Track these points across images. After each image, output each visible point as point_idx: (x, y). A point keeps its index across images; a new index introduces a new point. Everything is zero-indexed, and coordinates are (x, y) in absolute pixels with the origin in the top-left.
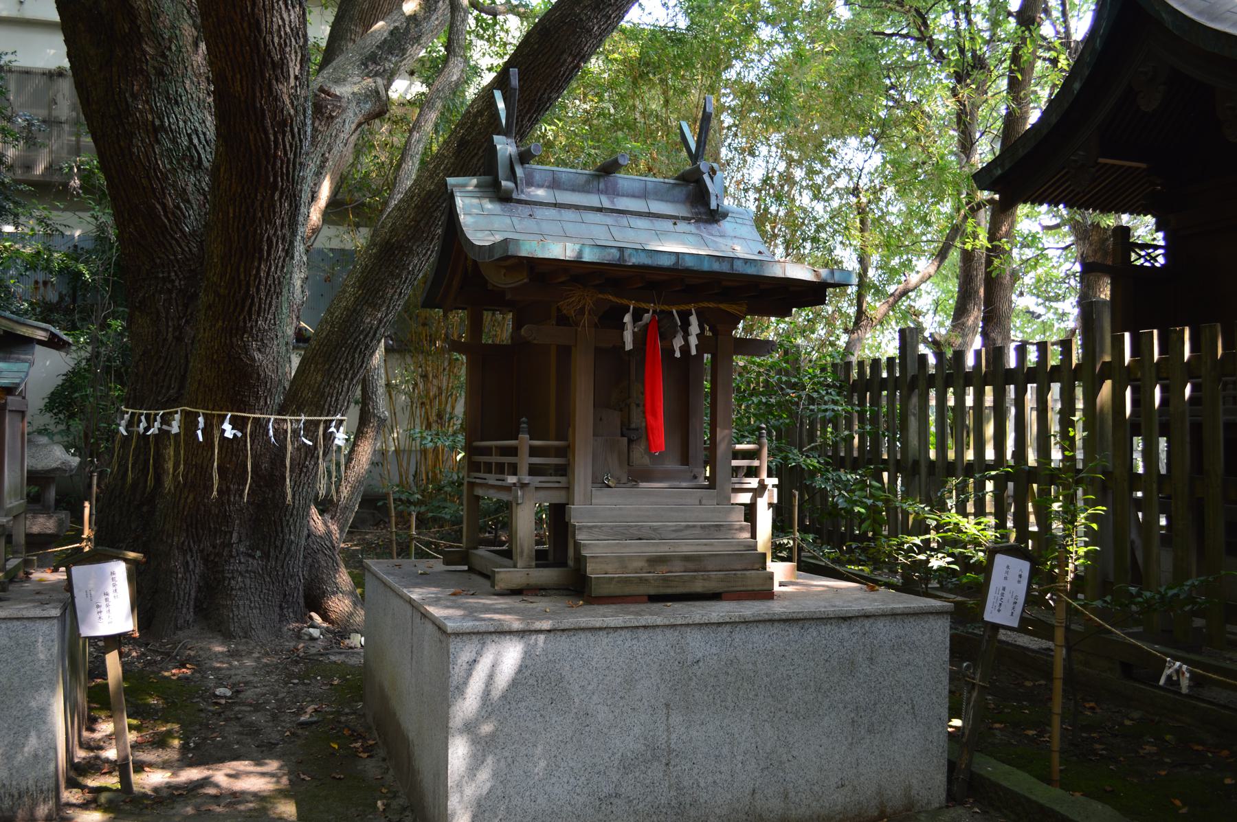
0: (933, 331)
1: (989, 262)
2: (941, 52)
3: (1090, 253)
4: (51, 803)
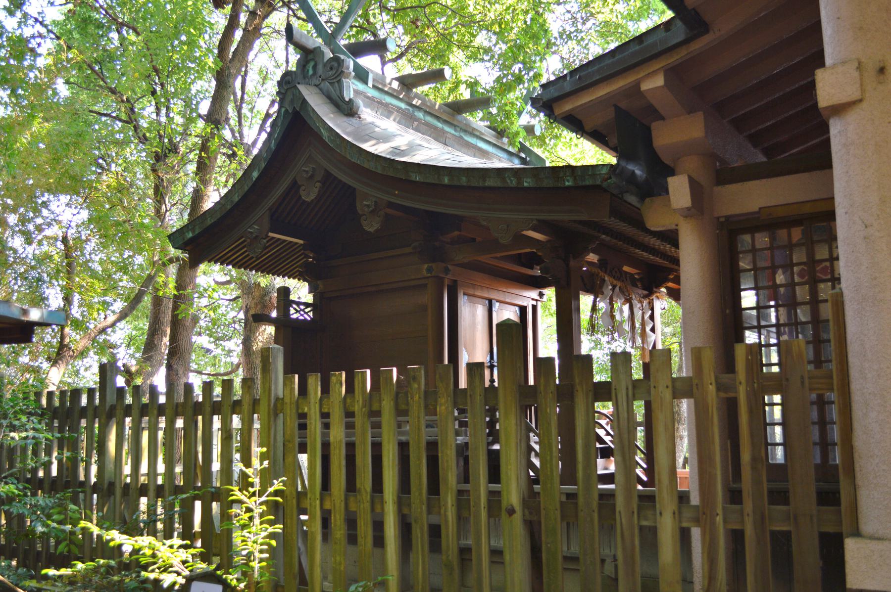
0: (125, 361)
1: (176, 307)
2: (144, 135)
3: (253, 305)
4: (144, 124)
